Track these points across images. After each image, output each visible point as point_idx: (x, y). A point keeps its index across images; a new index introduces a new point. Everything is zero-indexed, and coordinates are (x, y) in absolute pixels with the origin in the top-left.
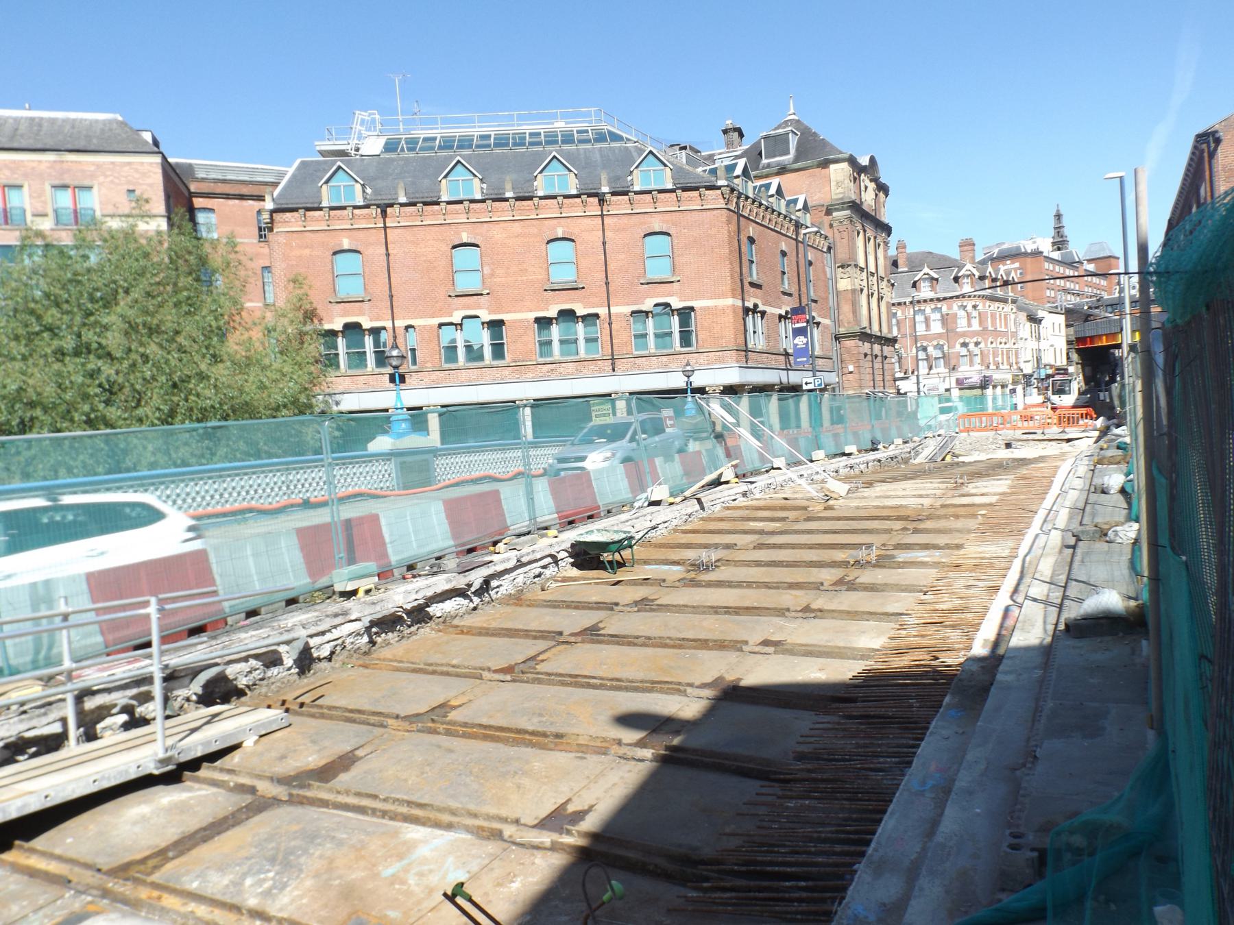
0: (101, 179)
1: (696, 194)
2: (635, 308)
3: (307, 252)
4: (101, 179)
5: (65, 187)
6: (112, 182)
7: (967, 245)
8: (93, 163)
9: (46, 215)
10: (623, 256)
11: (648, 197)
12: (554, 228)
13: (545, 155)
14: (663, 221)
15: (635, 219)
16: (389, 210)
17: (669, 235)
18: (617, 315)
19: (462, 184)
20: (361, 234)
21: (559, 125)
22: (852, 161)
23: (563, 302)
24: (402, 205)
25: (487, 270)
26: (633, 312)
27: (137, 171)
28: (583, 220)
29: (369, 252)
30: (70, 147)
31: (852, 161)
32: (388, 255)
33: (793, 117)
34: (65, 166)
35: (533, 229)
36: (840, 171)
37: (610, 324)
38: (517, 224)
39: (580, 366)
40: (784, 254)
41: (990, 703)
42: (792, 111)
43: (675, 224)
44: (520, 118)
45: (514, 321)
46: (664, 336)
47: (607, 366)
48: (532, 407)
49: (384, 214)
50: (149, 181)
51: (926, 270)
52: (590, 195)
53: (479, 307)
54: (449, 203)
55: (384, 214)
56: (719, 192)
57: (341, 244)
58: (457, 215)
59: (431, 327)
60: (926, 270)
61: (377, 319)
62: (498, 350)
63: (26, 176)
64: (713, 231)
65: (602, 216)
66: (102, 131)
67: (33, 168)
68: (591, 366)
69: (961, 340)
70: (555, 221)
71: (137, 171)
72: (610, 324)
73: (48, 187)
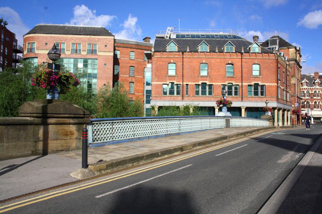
0: (99, 42)
1: (267, 54)
2: (249, 84)
3: (162, 63)
4: (99, 42)
6: (101, 43)
7: (316, 73)
8: (98, 38)
9: (70, 50)
11: (254, 54)
12: (228, 61)
13: (228, 41)
15: (250, 60)
16: (184, 53)
18: (244, 85)
19: (203, 47)
20: (176, 59)
21: (221, 33)
22: (295, 48)
23: (230, 81)
24: (188, 52)
27: (108, 40)
28: (236, 59)
30: (93, 34)
31: (295, 48)
32: (183, 65)
33: (276, 35)
34: (91, 39)
36: (292, 50)
37: (242, 88)
38: (218, 59)
40: (284, 72)
42: (276, 33)
44: (211, 31)
45: (216, 85)
49: (183, 54)
50: (110, 43)
51: (305, 80)
52: (239, 53)
54: (201, 52)
55: (183, 54)
56: (273, 54)
57: (203, 62)
58: (228, 56)
59: (193, 85)
60: (305, 80)
61: (178, 82)
63: (82, 42)
64: (271, 65)
66: (100, 30)
67: (84, 39)
69: (315, 101)
70: (229, 59)
71: (108, 40)
72: (242, 88)
73: (87, 45)
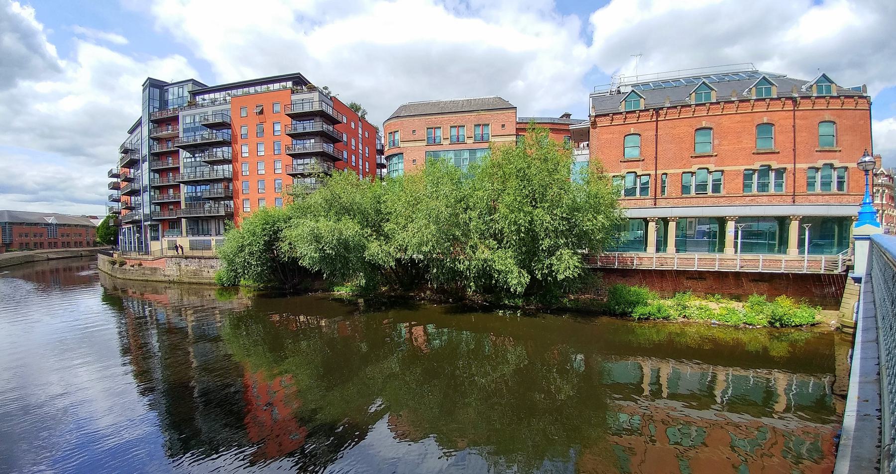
2: (811, 165)
5: (480, 125)
10: (805, 134)
14: (832, 115)
17: (834, 123)
25: (716, 142)
26: (809, 168)
29: (644, 134)
35: (748, 118)
37: (794, 174)
39: (771, 198)
41: (459, 317)
43: (839, 117)
46: (826, 184)
47: (790, 199)
48: (737, 222)
53: (709, 163)
59: (678, 174)
62: (716, 188)
65: (794, 110)
68: (779, 198)
